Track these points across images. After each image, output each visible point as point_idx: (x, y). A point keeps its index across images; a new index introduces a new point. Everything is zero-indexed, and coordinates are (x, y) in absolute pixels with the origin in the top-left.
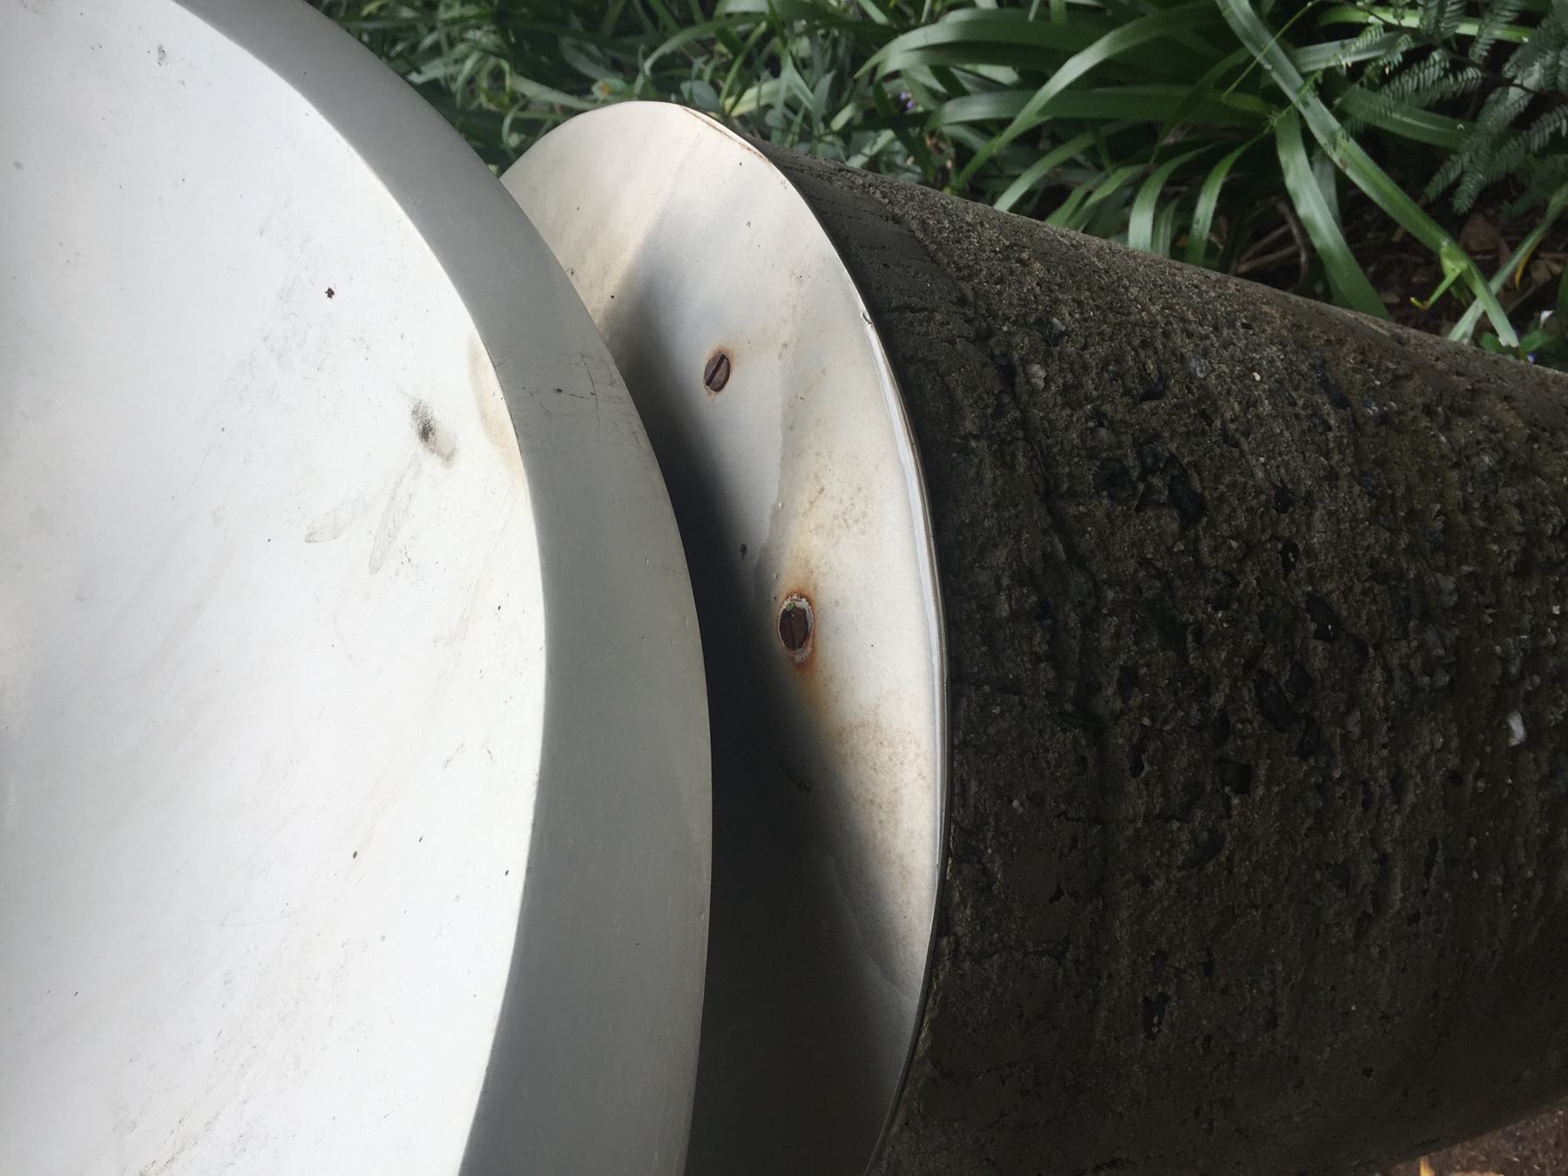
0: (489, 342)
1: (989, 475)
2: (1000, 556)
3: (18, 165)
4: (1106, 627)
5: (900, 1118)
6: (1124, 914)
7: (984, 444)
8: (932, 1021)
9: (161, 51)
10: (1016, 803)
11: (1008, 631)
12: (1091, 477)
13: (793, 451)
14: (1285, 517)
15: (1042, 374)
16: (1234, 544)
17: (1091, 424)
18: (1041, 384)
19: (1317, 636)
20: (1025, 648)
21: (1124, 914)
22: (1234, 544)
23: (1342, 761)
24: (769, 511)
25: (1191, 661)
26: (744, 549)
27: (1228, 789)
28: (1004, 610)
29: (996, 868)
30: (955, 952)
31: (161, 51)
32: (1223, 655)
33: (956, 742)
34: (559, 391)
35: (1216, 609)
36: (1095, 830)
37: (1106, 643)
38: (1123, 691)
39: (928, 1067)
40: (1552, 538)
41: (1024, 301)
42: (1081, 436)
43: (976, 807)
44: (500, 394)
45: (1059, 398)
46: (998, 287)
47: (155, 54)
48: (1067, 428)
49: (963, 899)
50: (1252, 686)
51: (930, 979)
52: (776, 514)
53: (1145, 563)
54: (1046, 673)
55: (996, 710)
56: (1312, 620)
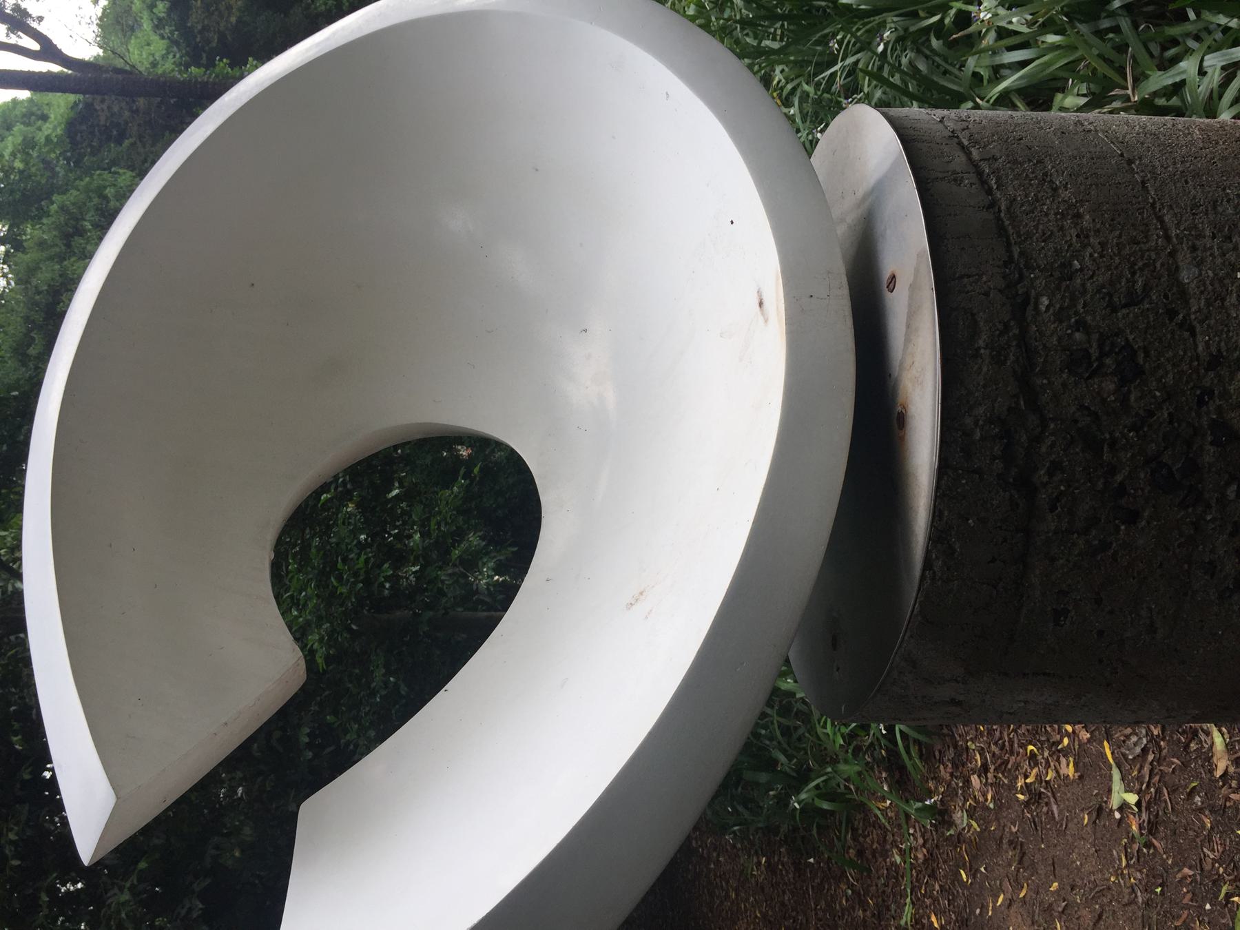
0: (783, 272)
1: (985, 369)
2: (980, 410)
3: (614, 137)
4: (1046, 441)
5: (908, 634)
6: (1038, 572)
7: (988, 352)
8: (920, 602)
9: (667, 94)
10: (970, 521)
11: (978, 446)
12: (1059, 362)
13: (908, 340)
14: (1211, 374)
15: (1046, 303)
16: (1158, 394)
17: (1069, 331)
18: (1043, 309)
19: (1212, 443)
20: (988, 453)
21: (1038, 572)
22: (1158, 394)
23: (1215, 511)
24: (898, 364)
25: (1105, 458)
26: (890, 375)
27: (1117, 522)
28: (978, 435)
29: (957, 546)
30: (933, 579)
31: (667, 94)
32: (1129, 456)
33: (938, 494)
34: (812, 296)
35: (1130, 431)
36: (1019, 535)
37: (1044, 449)
38: (1050, 474)
39: (920, 618)
40: (327, 667)
41: (1057, 252)
42: (1060, 340)
43: (947, 523)
44: (783, 301)
45: (1052, 317)
46: (1043, 244)
47: (665, 96)
48: (1052, 335)
49: (937, 558)
50: (1149, 471)
51: (920, 585)
52: (901, 364)
53: (1082, 407)
54: (998, 465)
55: (964, 482)
56: (1211, 435)
